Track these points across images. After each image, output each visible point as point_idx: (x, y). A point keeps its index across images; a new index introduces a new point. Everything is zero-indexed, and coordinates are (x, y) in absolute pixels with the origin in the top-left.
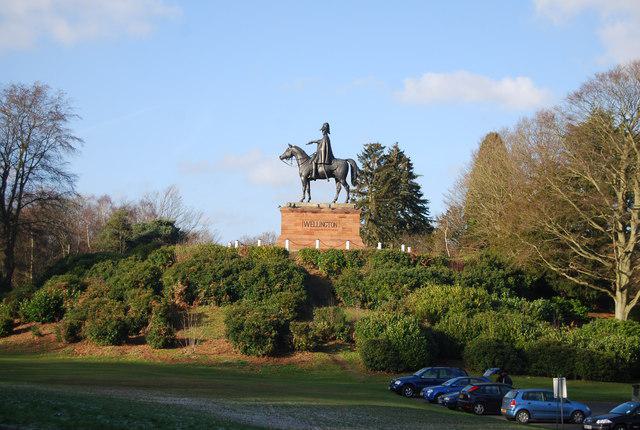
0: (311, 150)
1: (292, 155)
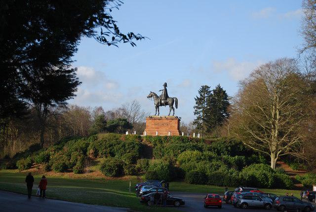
0: (159, 94)
1: (152, 96)
